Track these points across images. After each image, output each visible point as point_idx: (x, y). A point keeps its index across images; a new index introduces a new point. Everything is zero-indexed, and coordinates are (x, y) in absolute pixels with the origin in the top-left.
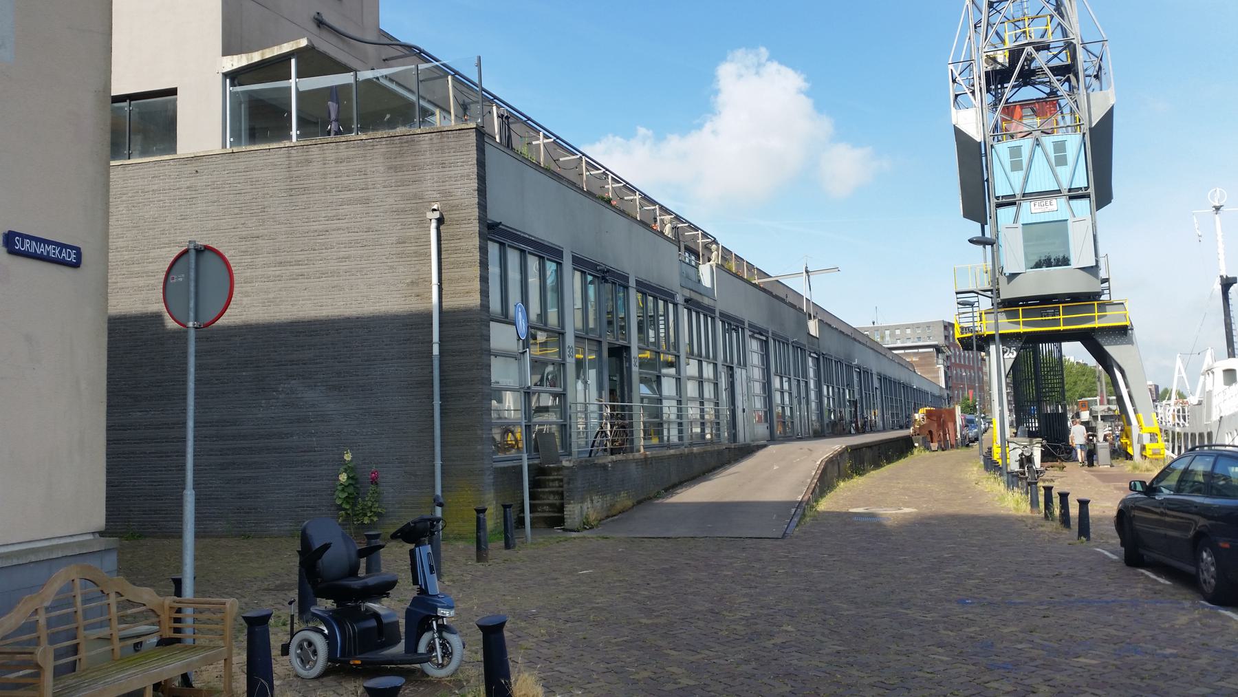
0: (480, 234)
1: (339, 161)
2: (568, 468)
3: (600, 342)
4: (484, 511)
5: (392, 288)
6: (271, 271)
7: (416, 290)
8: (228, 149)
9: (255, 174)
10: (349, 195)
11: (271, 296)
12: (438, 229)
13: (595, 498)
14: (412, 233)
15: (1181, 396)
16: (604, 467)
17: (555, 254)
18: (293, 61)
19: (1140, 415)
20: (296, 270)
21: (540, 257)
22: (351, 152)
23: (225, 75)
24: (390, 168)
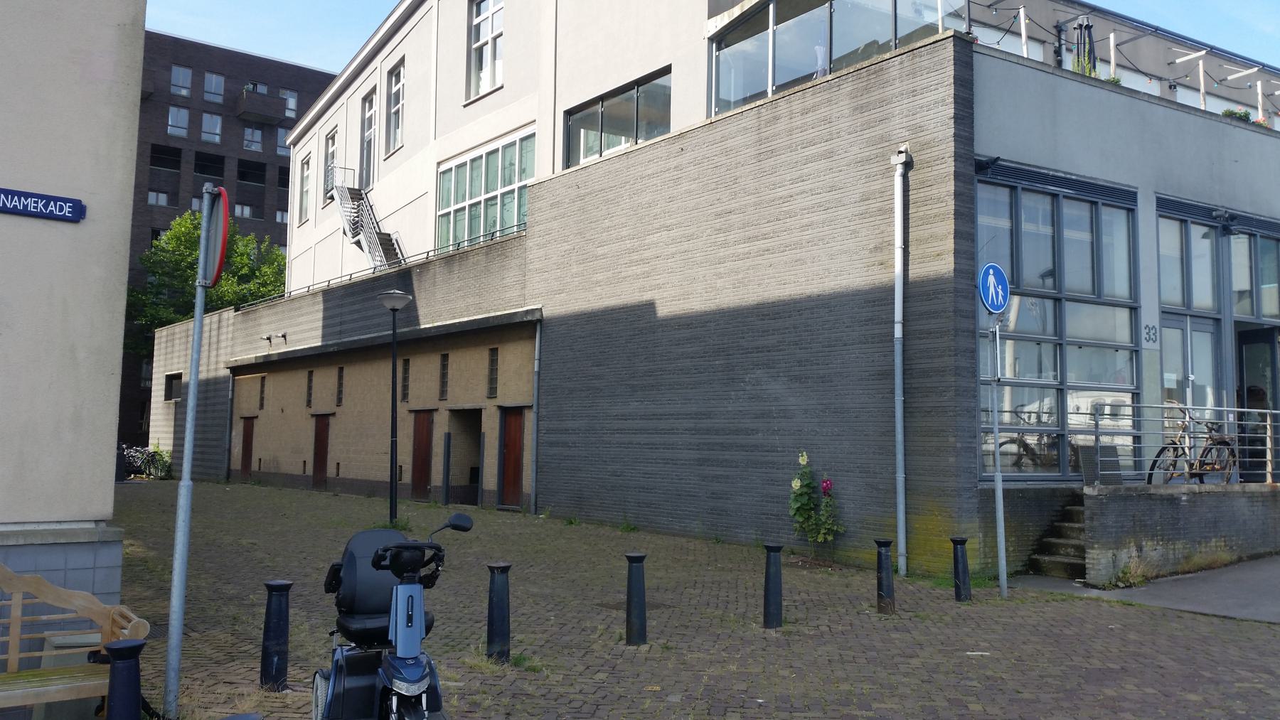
0: (957, 176)
1: (805, 112)
2: (1090, 497)
3: (1218, 321)
4: (963, 542)
5: (855, 257)
6: (742, 248)
8: (714, 118)
9: (730, 143)
12: (905, 177)
13: (1148, 545)
14: (876, 186)
16: (1172, 500)
17: (1124, 199)
18: (771, 7)
21: (1182, 221)
23: (711, 39)
24: (856, 109)
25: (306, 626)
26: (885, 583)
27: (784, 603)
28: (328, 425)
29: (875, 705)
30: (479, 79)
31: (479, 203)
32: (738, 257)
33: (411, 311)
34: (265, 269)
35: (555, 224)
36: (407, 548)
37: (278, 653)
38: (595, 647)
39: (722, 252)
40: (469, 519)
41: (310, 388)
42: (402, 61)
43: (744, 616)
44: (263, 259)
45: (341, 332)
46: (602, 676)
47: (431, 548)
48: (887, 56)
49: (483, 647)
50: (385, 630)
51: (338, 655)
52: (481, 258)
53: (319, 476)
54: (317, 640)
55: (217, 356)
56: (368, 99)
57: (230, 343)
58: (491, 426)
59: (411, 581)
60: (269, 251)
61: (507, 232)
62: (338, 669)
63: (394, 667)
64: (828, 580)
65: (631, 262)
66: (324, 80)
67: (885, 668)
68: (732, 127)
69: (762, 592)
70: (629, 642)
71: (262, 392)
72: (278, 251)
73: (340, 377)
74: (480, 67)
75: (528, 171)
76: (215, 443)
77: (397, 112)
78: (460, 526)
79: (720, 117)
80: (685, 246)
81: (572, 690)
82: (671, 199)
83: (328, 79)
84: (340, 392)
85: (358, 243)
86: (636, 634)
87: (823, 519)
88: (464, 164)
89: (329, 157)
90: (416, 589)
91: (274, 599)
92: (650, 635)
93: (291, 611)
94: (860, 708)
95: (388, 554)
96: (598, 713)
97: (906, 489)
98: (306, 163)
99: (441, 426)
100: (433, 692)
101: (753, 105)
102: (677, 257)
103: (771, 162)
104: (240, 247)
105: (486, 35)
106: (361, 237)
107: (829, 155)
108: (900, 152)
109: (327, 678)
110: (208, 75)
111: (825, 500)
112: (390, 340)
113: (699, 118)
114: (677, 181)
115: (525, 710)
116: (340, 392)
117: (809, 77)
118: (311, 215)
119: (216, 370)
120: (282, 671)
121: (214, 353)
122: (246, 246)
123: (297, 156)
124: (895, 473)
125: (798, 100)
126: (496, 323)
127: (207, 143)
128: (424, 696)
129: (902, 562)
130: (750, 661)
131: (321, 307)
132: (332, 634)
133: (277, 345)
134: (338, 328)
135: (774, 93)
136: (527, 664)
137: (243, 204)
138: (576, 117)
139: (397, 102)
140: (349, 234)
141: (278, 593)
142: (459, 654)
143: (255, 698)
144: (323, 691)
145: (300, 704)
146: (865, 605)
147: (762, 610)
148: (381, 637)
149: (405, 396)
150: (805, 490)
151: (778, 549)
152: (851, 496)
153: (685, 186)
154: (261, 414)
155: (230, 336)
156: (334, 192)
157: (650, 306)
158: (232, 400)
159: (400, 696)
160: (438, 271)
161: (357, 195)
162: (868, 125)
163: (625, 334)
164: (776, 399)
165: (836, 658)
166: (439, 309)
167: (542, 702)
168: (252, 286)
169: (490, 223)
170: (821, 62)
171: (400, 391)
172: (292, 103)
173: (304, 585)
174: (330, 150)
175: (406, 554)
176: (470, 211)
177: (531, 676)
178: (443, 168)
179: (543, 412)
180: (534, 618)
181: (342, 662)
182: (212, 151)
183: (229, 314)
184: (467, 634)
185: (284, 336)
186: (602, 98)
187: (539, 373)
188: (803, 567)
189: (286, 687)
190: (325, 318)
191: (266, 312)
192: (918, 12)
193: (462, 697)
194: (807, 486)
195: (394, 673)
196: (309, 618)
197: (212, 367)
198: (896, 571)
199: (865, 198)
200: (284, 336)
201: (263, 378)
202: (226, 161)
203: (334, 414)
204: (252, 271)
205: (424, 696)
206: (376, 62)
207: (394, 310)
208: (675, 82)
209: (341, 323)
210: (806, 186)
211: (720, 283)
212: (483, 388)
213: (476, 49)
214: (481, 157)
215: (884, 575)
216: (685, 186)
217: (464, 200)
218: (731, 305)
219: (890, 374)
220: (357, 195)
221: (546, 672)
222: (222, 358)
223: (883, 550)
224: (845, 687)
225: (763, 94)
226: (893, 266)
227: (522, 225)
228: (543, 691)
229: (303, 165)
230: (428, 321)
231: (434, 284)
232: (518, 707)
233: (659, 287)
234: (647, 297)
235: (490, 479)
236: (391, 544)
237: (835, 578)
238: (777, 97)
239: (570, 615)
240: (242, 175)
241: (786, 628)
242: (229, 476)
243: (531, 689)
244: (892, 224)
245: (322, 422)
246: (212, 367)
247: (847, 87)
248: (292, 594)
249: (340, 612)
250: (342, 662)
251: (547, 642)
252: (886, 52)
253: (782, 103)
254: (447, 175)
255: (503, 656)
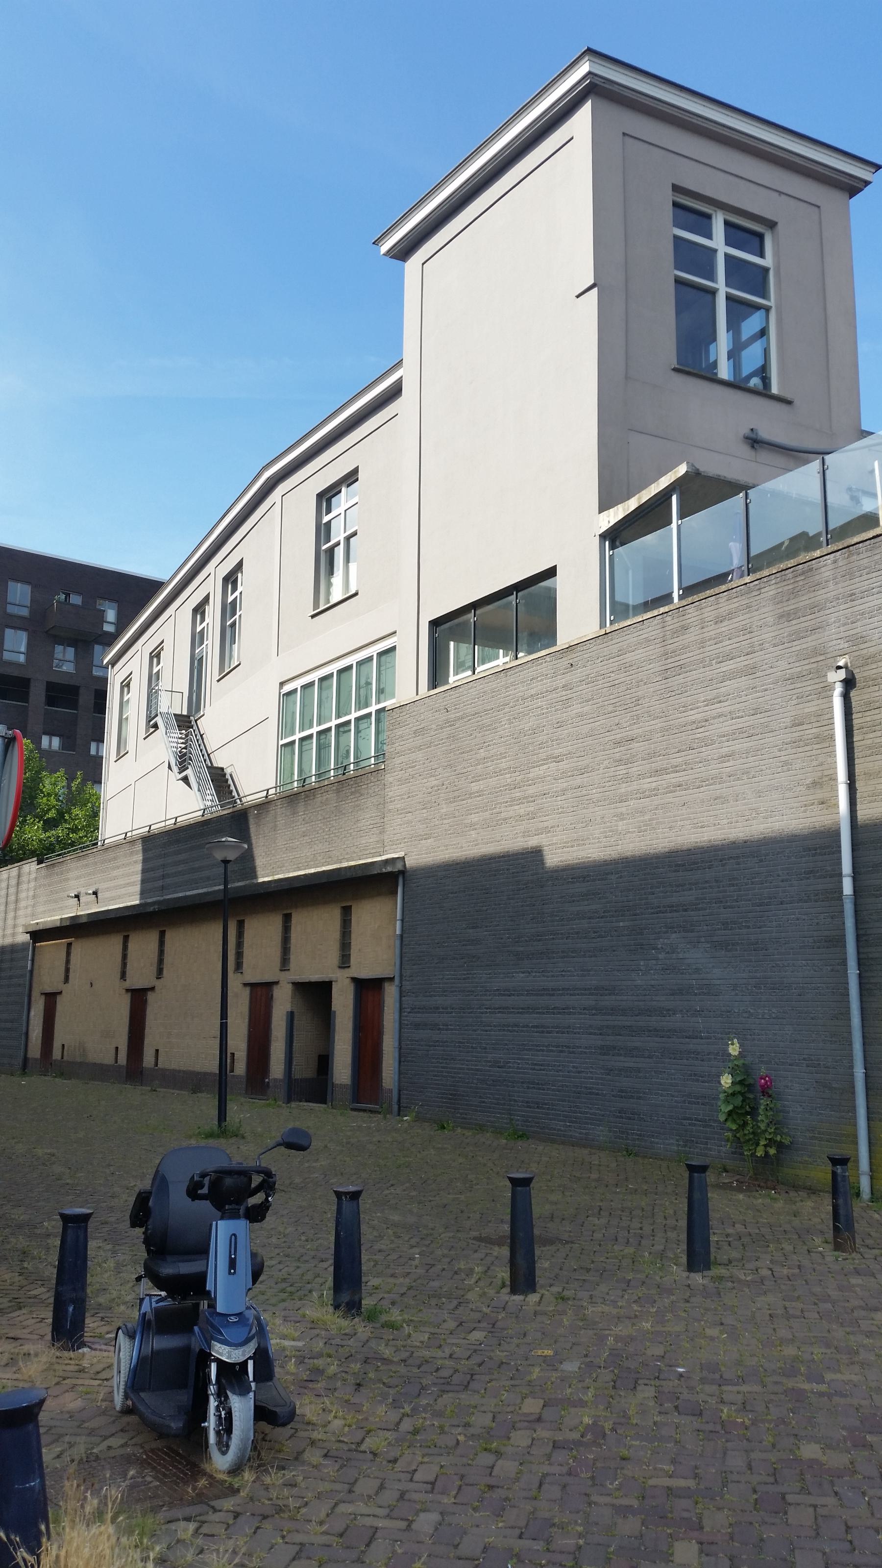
1: (719, 620)
5: (788, 794)
6: (647, 784)
7: (820, 794)
9: (629, 657)
10: (729, 666)
11: (647, 817)
12: (846, 697)
14: (811, 708)
15: (145, 1559)
18: (674, 498)
19: (353, 566)
20: (673, 778)
22: (734, 605)
23: (603, 537)
25: (111, 1264)
26: (842, 1212)
27: (714, 1238)
28: (145, 1002)
29: (829, 1376)
30: (329, 585)
31: (329, 729)
32: (643, 794)
33: (247, 861)
34: (76, 811)
35: (420, 755)
36: (230, 1172)
37: (73, 1301)
38: (470, 1296)
39: (624, 789)
40: (307, 1135)
41: (125, 957)
42: (239, 566)
43: (662, 1255)
44: (73, 799)
45: (163, 888)
46: (478, 1335)
47: (259, 1172)
48: (817, 553)
49: (328, 1294)
50: (202, 1278)
51: (146, 1307)
52: (331, 796)
53: (134, 1069)
54: (120, 1283)
55: (15, 918)
56: (199, 610)
57: (31, 902)
58: (343, 1003)
59: (234, 1215)
60: (81, 790)
61: (363, 764)
62: (145, 1324)
63: (213, 1326)
64: (771, 1207)
65: (513, 800)
66: (146, 589)
67: (842, 1325)
68: (631, 638)
69: (683, 1223)
70: (514, 1291)
71: (68, 962)
72: (89, 788)
73: (162, 943)
74: (331, 571)
75: (387, 690)
76: (9, 1025)
77: (233, 625)
78: (296, 1143)
79: (616, 626)
80: (578, 781)
81: (440, 1354)
82: (560, 725)
83: (155, 586)
84: (161, 961)
85: (185, 780)
86: (523, 1280)
87: (763, 1126)
88: (311, 684)
89: (153, 678)
90: (240, 1226)
91: (69, 1231)
92: (540, 1280)
93: (92, 1244)
94: (809, 1379)
95: (206, 1181)
96: (473, 1385)
97: (868, 1089)
98: (126, 685)
99: (283, 1002)
100: (262, 1358)
101: (655, 612)
102: (569, 794)
103: (680, 679)
104: (47, 785)
105: (338, 535)
106: (189, 772)
107: (751, 671)
108: (839, 668)
109: (131, 1336)
110: (11, 584)
111: (764, 1102)
112: (221, 897)
113: (590, 627)
114: (566, 702)
115: (380, 1380)
116: (161, 961)
117: (721, 578)
118: (131, 746)
119: (14, 935)
120: (78, 1325)
121: (11, 915)
122: (53, 784)
123: (115, 678)
124: (852, 1067)
125: (710, 607)
126: (349, 875)
127: (10, 664)
128: (250, 1364)
129: (865, 1183)
130: (669, 1316)
131: (139, 857)
132: (139, 1279)
133: (87, 904)
134: (160, 883)
135: (681, 598)
136: (384, 1318)
137: (51, 734)
138: (444, 628)
139: (234, 613)
140: (175, 769)
141: (75, 1226)
142: (298, 1303)
143: (44, 1359)
144: (126, 1353)
145: (99, 1367)
146: (818, 1240)
147: (684, 1247)
148: (195, 1286)
149: (239, 966)
150: (738, 1088)
151: (703, 1169)
152: (796, 1092)
153: (576, 709)
154: (67, 989)
155: (31, 893)
156: (159, 720)
157: (537, 854)
158: (32, 972)
159: (221, 1363)
160: (280, 812)
161: (185, 722)
162: (798, 636)
163: (510, 882)
164: (697, 971)
165: (780, 1311)
166: (278, 861)
167: (402, 1369)
168: (60, 832)
169: (342, 754)
170: (737, 559)
171: (231, 959)
172: (111, 615)
173: (111, 1209)
174: (155, 670)
175: (228, 1181)
176: (318, 739)
177: (388, 1334)
178: (287, 688)
179: (407, 985)
180: (394, 1256)
181: (150, 1316)
182: (16, 673)
183: (30, 867)
184: (309, 1276)
185: (95, 893)
186: (474, 606)
187: (402, 936)
188: (739, 1190)
189: (83, 1345)
190: (144, 871)
191: (73, 865)
192: (855, 500)
193: (301, 1360)
194: (741, 1083)
195: (213, 1333)
196: (114, 1252)
197: (9, 931)
198: (858, 1195)
199: (797, 723)
200: (95, 893)
201: (69, 945)
202: (32, 684)
203: (152, 989)
204: (61, 814)
205: (250, 1364)
206: (210, 567)
207: (226, 862)
208: (561, 583)
209: (163, 877)
210: (724, 708)
211: (621, 826)
212: (333, 956)
213: (326, 551)
214: (332, 675)
215: (841, 1201)
216: (576, 709)
217: (311, 726)
218: (637, 853)
219: (841, 941)
220: (185, 722)
221: (407, 1329)
222: (21, 921)
223: (839, 1169)
224: (790, 1351)
225: (666, 598)
226: (837, 805)
227: (380, 755)
228: (404, 1355)
229: (122, 688)
230: (267, 874)
231: (275, 828)
232: (371, 1375)
233: (547, 830)
234: (532, 842)
235: (342, 1069)
236: (211, 1167)
237: (779, 1205)
238: (684, 602)
239: (439, 1252)
240: (51, 701)
241: (715, 1271)
242: (25, 1066)
243: (387, 1352)
244: (832, 754)
245: (139, 998)
246: (9, 931)
247: (770, 591)
248: (91, 1225)
249: (149, 1251)
250: (150, 1316)
251: (410, 1288)
252: (815, 550)
253: (691, 609)
254: (291, 698)
255: (353, 1307)
